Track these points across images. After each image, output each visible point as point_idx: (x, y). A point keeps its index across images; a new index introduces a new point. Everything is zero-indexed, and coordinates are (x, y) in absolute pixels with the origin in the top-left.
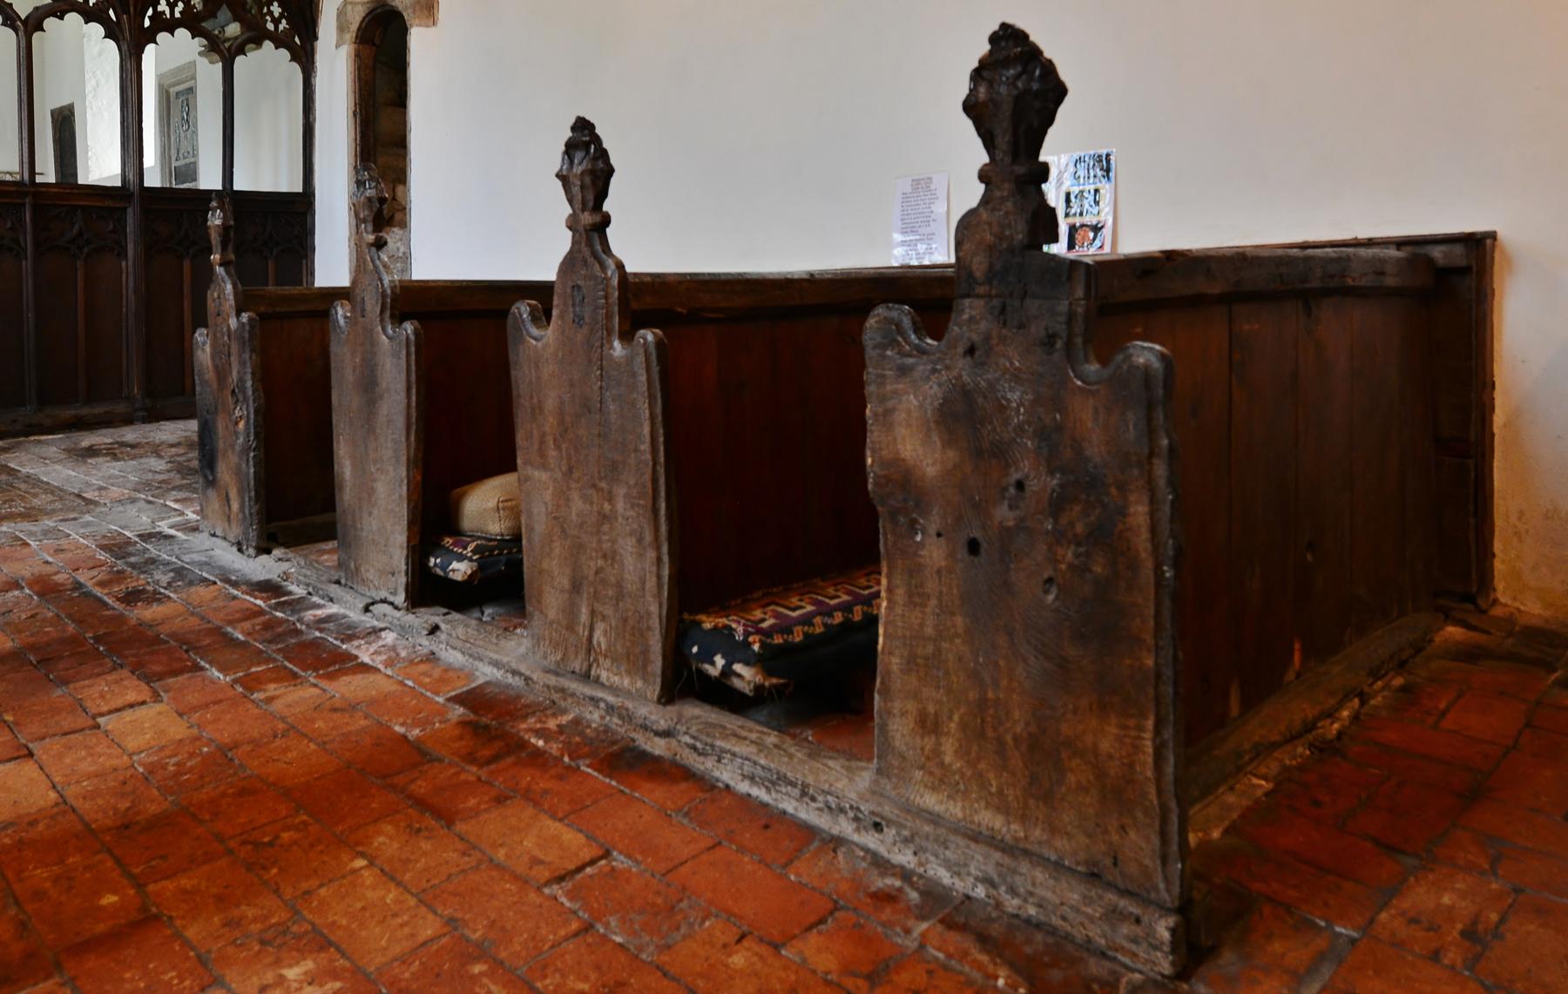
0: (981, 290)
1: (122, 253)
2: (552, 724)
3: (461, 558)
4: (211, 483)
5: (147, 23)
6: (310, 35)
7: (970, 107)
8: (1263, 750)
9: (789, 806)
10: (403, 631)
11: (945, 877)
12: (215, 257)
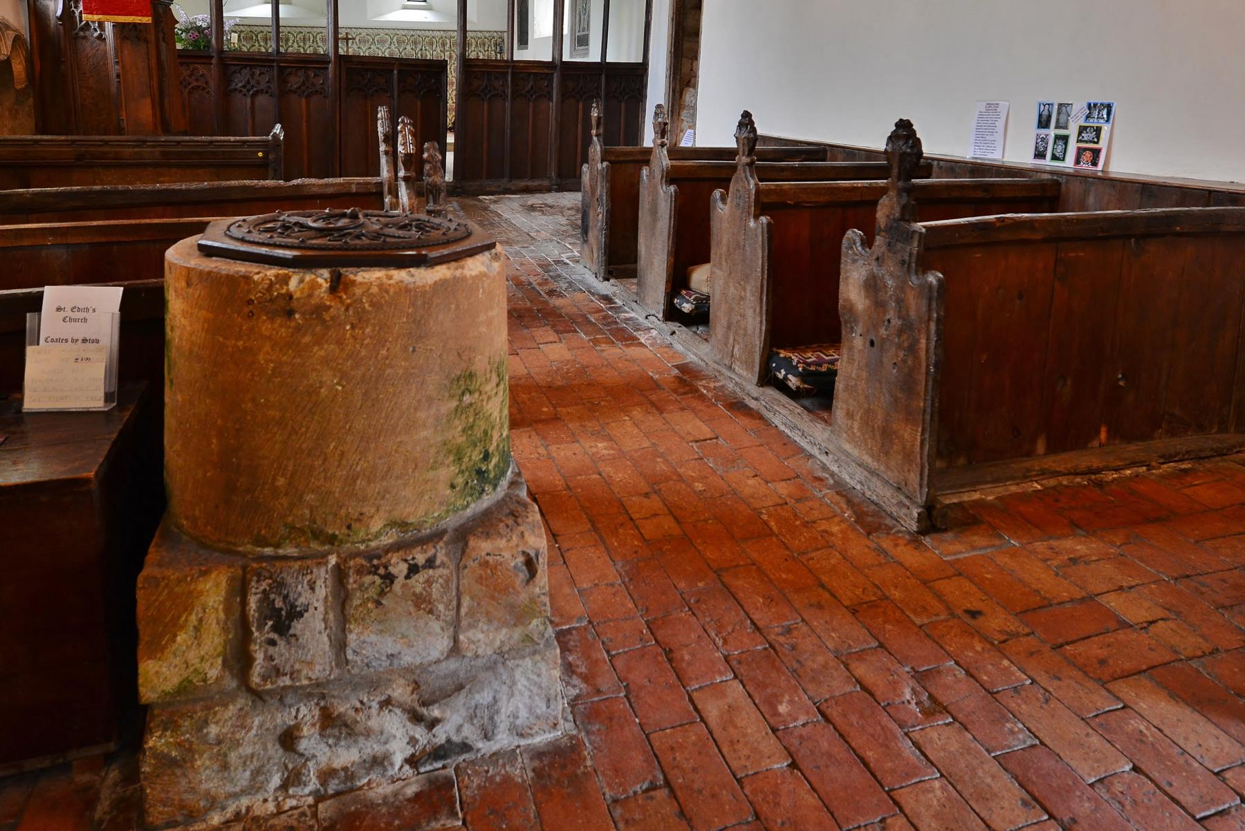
1: (551, 99)
2: (712, 385)
3: (688, 302)
8: (1044, 473)
9: (797, 439)
10: (660, 332)
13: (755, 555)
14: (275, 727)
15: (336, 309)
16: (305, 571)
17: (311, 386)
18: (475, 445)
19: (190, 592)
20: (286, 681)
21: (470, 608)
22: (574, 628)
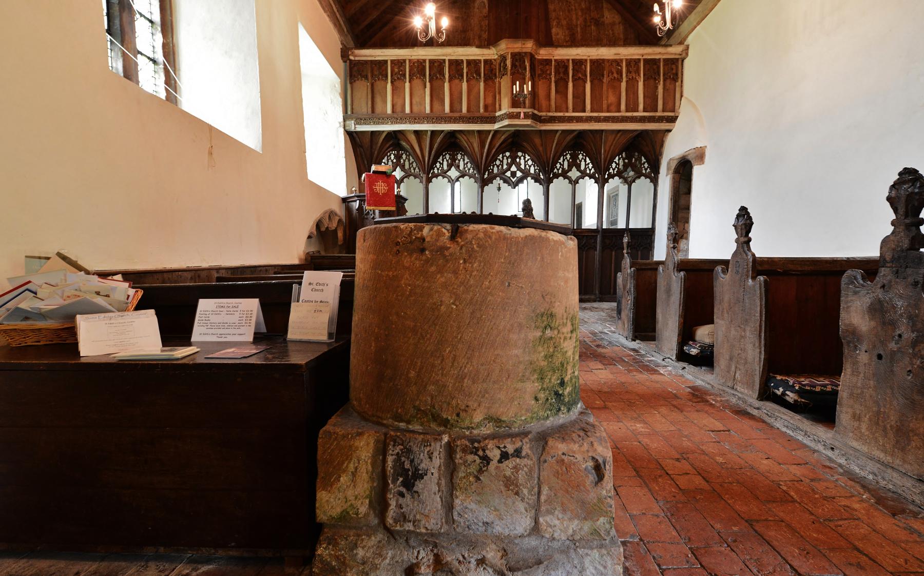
0: (888, 265)
4: (619, 319)
7: (889, 199)
9: (800, 438)
10: (674, 367)
11: (857, 470)
12: (625, 251)
13: (782, 514)
14: (403, 561)
15: (453, 248)
16: (425, 443)
17: (434, 304)
18: (554, 372)
19: (350, 446)
20: (409, 527)
21: (549, 497)
22: (629, 542)
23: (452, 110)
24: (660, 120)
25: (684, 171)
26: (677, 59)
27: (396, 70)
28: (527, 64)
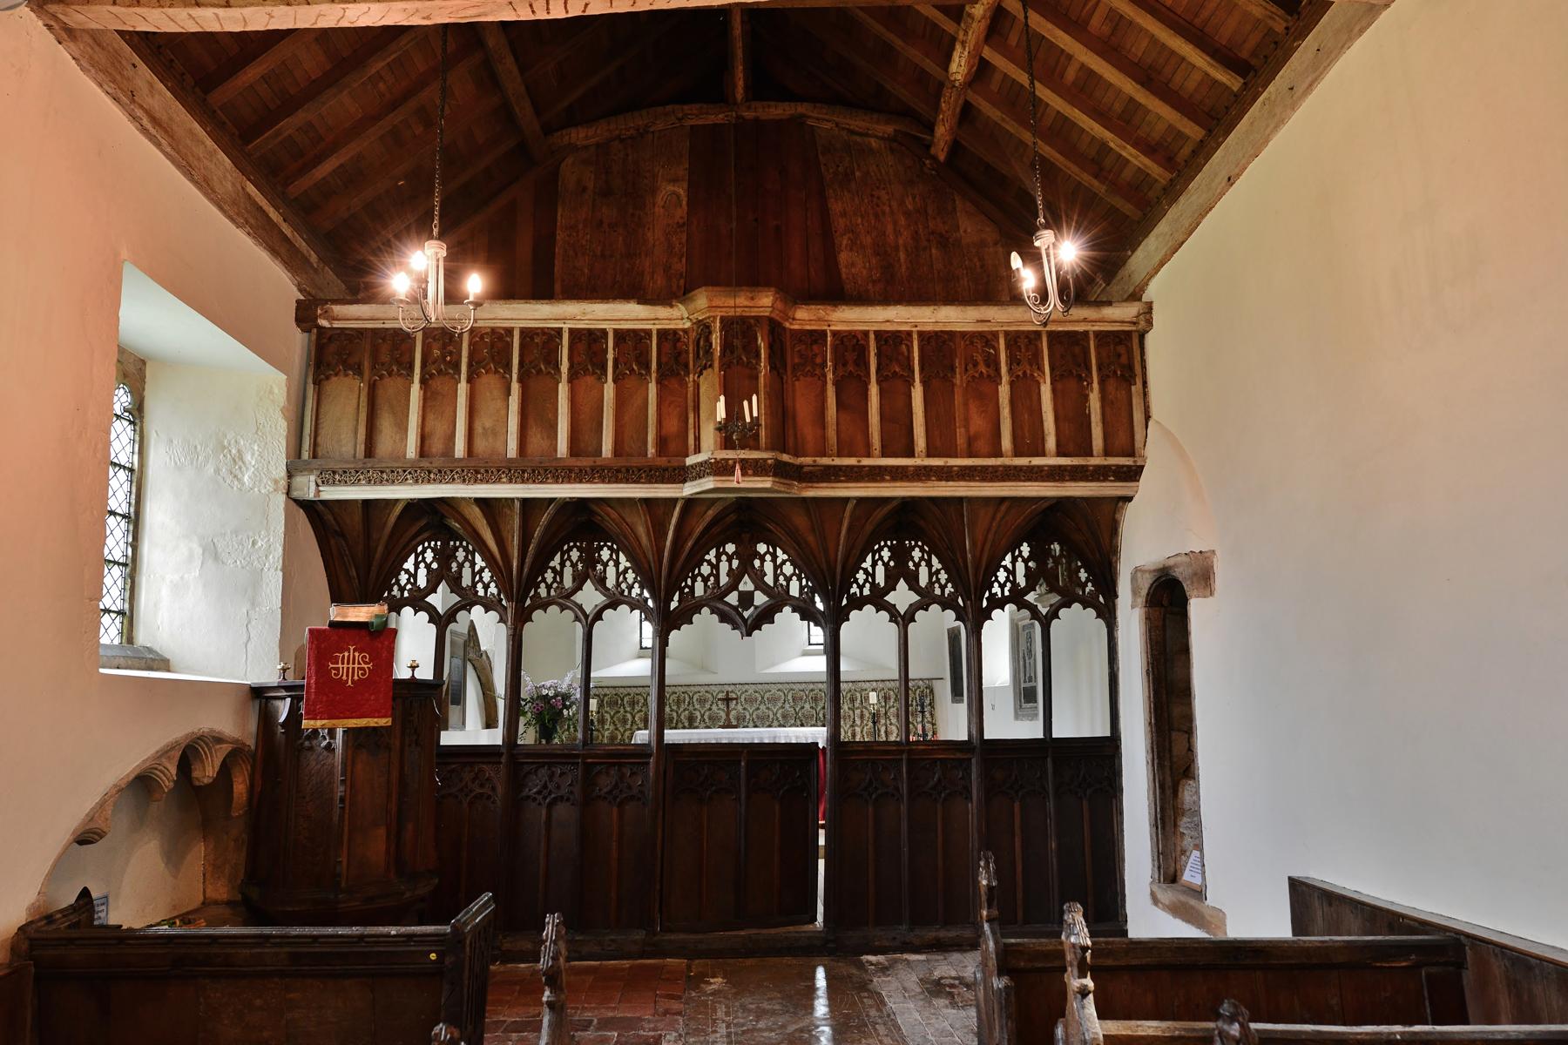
1: (969, 798)
5: (985, 604)
6: (1111, 594)
23: (574, 449)
24: (1100, 474)
25: (1168, 599)
26: (1129, 333)
27: (436, 352)
28: (762, 344)
